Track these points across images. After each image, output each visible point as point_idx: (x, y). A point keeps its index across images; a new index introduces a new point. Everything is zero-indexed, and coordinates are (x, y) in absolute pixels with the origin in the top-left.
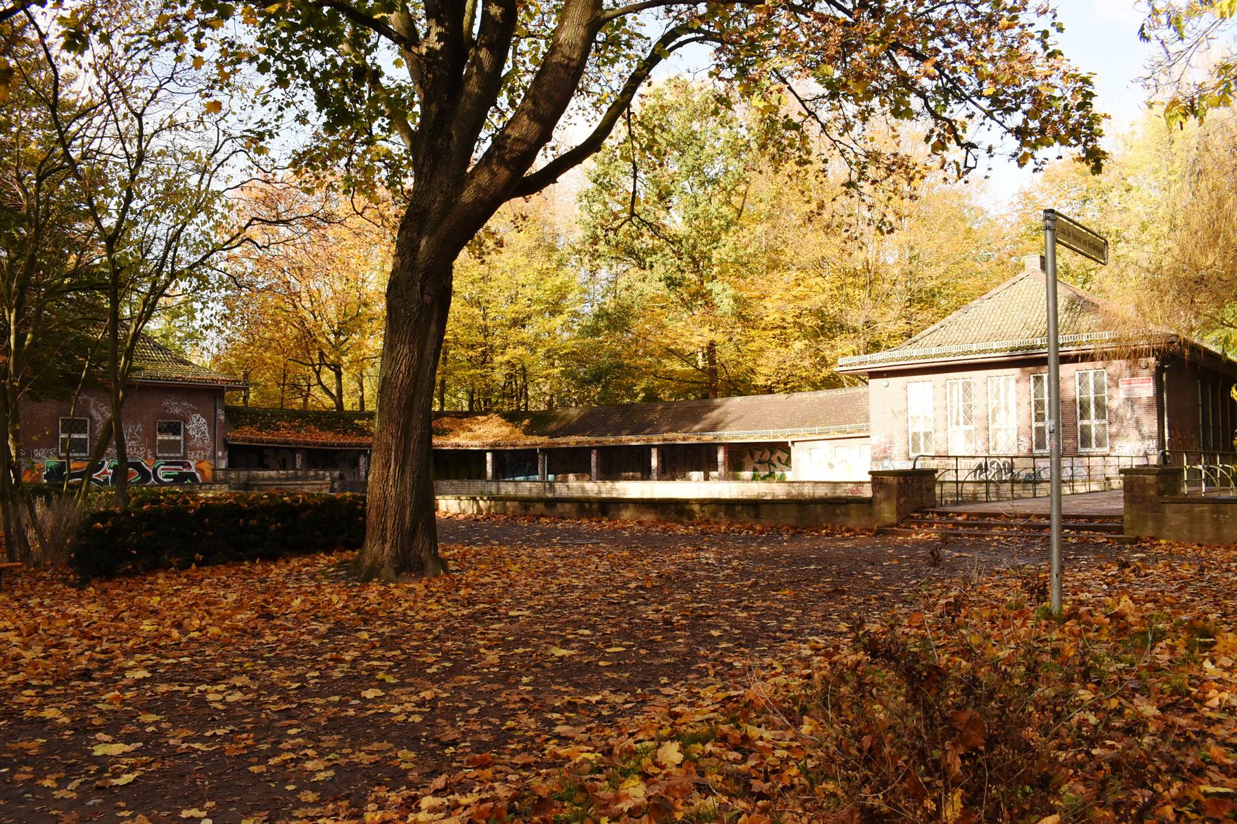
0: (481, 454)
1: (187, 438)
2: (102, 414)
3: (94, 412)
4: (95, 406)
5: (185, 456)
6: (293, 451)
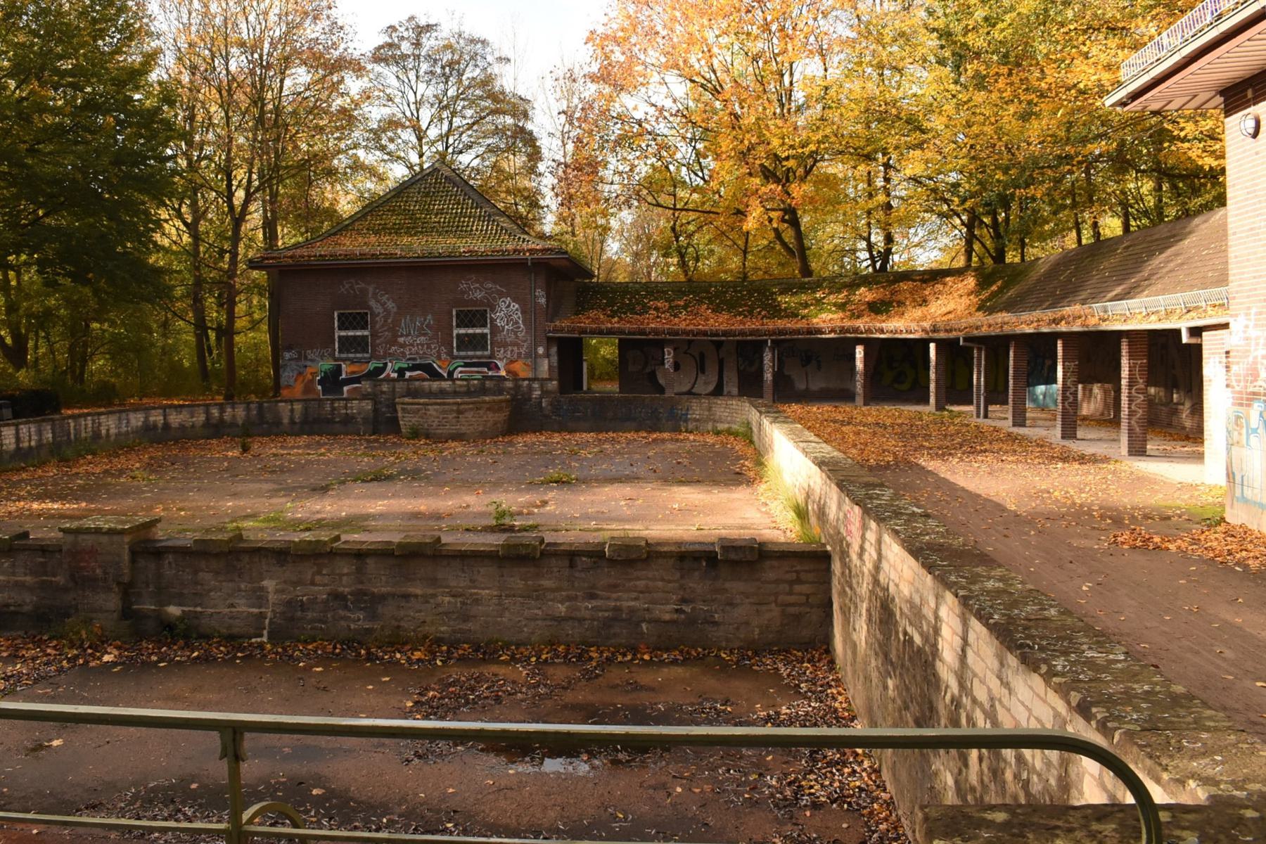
0: (924, 343)
1: (495, 330)
2: (383, 305)
3: (372, 303)
4: (375, 294)
5: (492, 356)
6: (660, 344)
